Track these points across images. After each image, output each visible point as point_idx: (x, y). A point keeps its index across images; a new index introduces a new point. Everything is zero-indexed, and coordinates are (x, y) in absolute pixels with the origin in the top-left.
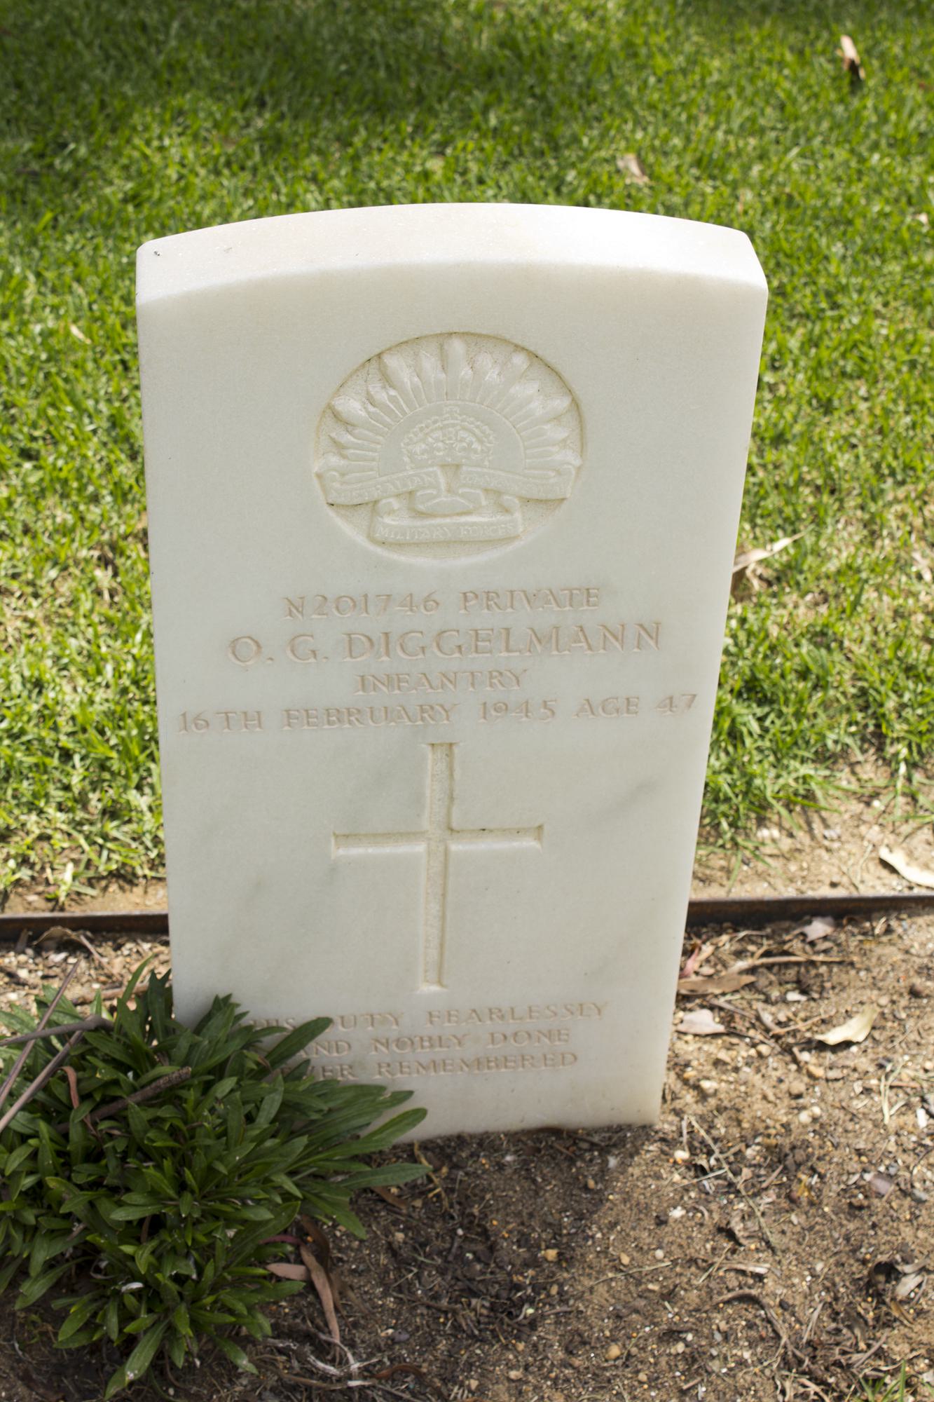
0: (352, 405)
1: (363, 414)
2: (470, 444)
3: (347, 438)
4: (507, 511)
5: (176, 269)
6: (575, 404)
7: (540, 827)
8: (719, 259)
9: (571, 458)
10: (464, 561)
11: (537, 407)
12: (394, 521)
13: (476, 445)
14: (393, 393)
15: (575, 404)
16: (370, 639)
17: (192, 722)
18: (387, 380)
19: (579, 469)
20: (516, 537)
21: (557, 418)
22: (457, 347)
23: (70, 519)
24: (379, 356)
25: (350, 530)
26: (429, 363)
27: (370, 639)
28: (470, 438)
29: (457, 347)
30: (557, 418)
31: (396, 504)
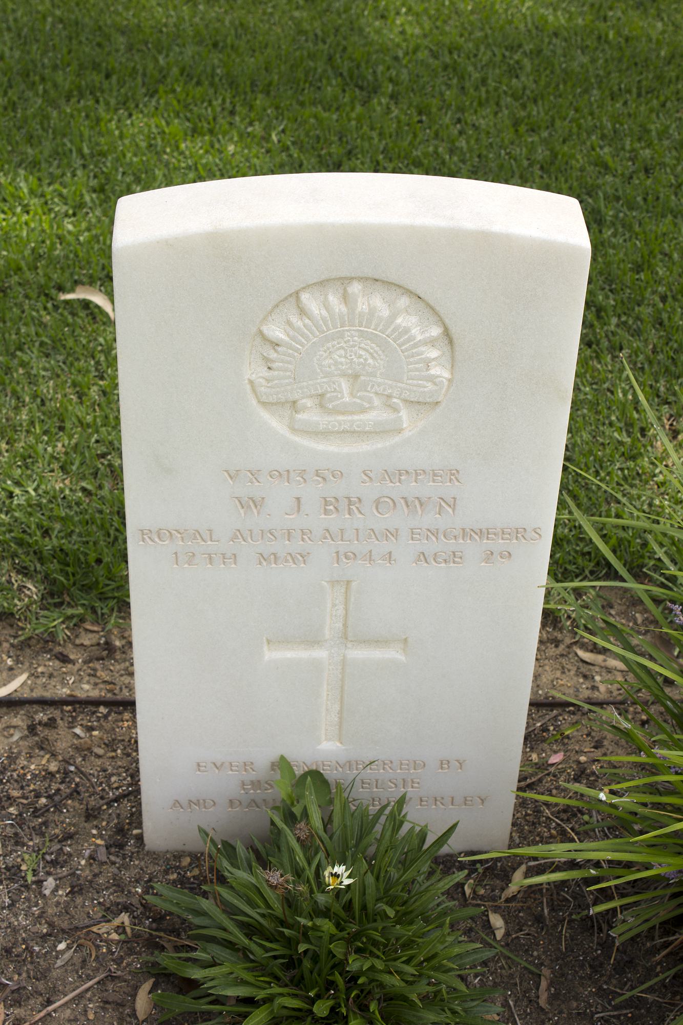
0: (276, 332)
1: (287, 339)
2: (366, 360)
3: (273, 355)
4: (396, 410)
5: (144, 220)
6: (447, 333)
7: (406, 640)
8: (554, 222)
9: (441, 372)
10: (365, 447)
11: (416, 333)
12: (311, 416)
13: (370, 361)
14: (307, 321)
15: (447, 333)
16: (354, 554)
17: (143, 533)
18: (302, 312)
19: (450, 380)
20: (400, 431)
21: (432, 342)
22: (355, 288)
23: (98, 965)
24: (297, 293)
25: (275, 423)
26: (334, 299)
27: (354, 554)
28: (368, 356)
29: (355, 288)
30: (432, 342)
31: (309, 403)
